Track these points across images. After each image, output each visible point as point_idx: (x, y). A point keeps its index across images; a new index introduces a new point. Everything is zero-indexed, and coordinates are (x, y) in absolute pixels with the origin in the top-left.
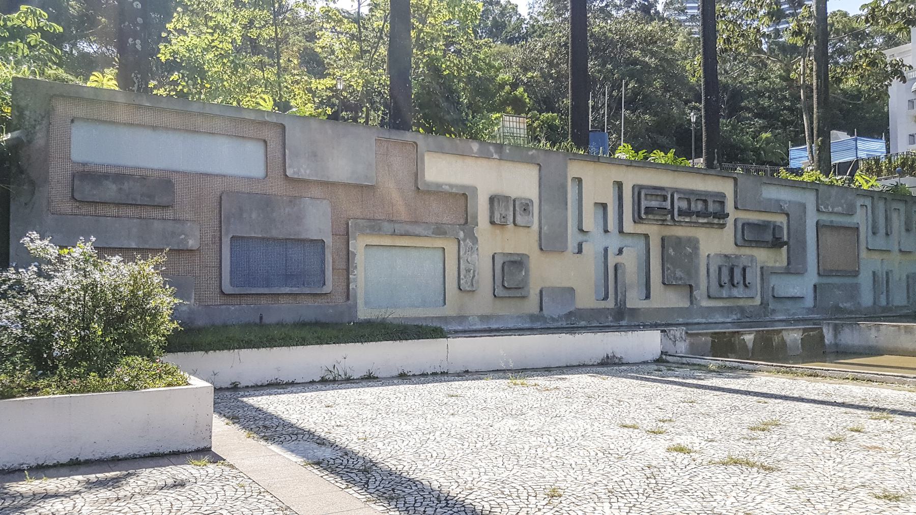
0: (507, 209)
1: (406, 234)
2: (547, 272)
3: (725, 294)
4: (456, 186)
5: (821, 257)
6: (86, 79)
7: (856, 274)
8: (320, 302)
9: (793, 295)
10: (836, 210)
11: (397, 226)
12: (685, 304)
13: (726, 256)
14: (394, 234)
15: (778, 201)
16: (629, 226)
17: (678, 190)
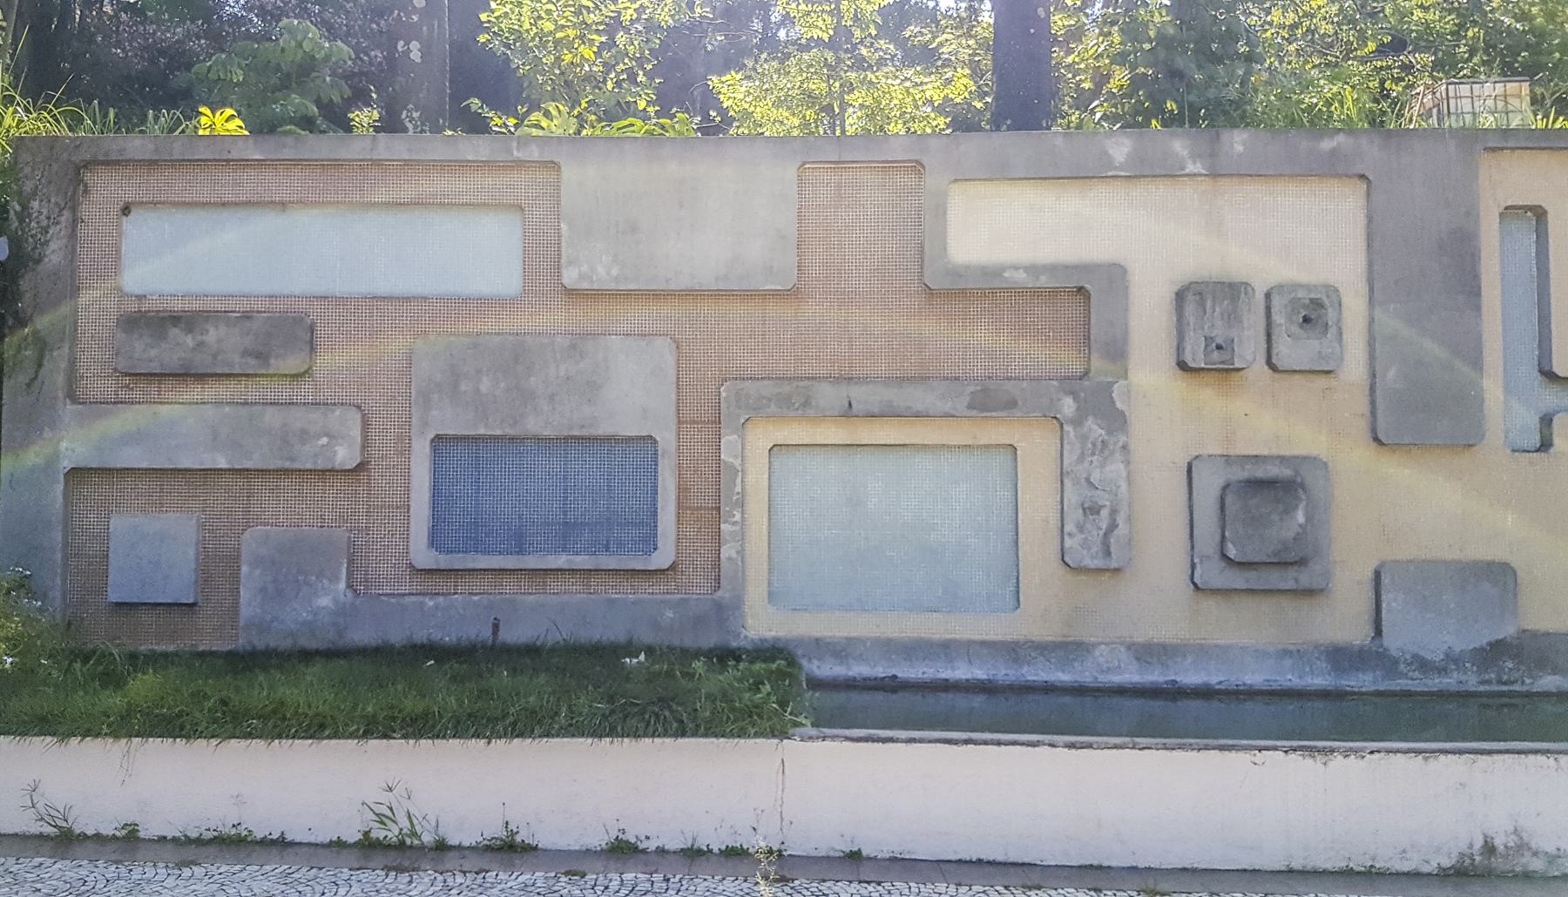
0: (1232, 318)
4: (1052, 269)
11: (858, 393)
14: (848, 413)
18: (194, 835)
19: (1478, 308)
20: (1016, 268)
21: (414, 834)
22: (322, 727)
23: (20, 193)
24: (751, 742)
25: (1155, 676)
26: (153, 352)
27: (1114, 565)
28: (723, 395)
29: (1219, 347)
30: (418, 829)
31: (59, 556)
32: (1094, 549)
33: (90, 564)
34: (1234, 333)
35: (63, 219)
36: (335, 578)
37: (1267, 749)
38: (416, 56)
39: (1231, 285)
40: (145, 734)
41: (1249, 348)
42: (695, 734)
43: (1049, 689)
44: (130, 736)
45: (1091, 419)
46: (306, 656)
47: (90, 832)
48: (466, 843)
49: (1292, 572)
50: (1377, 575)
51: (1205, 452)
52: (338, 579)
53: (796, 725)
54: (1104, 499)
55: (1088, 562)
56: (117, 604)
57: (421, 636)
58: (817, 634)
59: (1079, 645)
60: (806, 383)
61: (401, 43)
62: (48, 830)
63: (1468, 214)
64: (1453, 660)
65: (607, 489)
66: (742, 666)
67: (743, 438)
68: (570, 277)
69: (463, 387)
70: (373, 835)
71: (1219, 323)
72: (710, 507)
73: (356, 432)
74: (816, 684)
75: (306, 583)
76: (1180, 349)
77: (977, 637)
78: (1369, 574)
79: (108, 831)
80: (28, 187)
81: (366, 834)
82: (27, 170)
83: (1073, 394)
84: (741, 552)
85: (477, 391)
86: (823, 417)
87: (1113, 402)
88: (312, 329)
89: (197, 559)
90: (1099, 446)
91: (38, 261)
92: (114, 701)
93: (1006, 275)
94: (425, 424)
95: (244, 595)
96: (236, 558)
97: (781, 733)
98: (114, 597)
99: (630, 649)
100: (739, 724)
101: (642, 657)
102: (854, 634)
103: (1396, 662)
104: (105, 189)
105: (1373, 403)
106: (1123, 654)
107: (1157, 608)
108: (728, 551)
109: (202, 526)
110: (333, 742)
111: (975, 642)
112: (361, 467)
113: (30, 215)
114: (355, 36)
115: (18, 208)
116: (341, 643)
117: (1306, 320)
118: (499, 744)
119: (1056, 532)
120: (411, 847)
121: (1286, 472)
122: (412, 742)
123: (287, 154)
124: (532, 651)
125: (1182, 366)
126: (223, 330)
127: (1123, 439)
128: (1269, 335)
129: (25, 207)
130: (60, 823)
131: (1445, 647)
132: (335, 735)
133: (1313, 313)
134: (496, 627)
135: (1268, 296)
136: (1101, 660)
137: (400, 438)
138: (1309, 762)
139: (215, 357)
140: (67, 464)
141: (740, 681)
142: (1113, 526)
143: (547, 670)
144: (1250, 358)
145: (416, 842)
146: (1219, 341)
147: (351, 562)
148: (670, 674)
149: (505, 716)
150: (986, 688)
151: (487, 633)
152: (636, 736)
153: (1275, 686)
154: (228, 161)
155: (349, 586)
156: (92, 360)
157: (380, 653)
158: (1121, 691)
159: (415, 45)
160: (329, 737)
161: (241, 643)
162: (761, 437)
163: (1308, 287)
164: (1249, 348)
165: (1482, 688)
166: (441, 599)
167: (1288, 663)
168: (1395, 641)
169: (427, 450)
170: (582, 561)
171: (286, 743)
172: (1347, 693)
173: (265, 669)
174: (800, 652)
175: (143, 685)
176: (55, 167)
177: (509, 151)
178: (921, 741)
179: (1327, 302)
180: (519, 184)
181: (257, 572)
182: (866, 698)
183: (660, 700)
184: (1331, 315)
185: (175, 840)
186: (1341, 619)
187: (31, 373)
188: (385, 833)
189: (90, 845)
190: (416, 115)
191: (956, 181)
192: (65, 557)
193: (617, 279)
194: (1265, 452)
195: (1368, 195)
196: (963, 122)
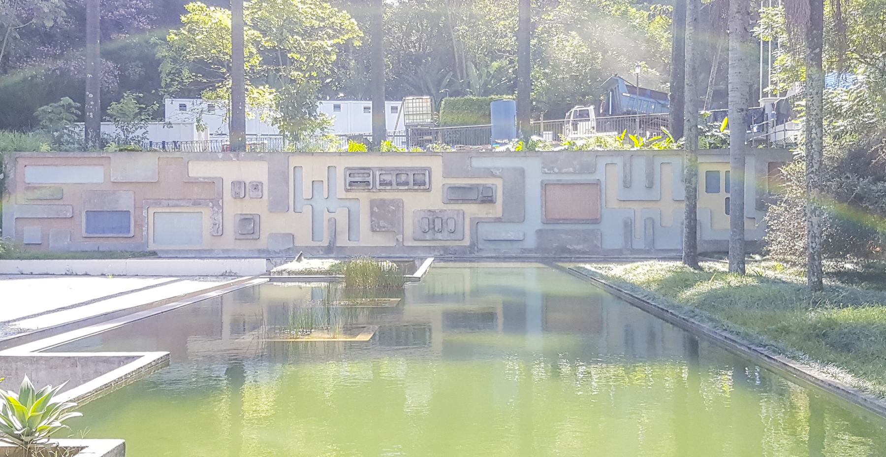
0: (240, 188)
1: (176, 206)
2: (273, 224)
3: (428, 237)
4: (208, 178)
5: (251, 255)
6: (690, 26)
7: (596, 221)
8: (128, 241)
9: (505, 238)
10: (564, 170)
11: (170, 202)
12: (393, 244)
13: (430, 211)
14: (168, 206)
15: (489, 169)
16: (341, 193)
17: (381, 169)
86: (163, 207)
104: (21, 162)
133: (257, 186)
170: (115, 235)
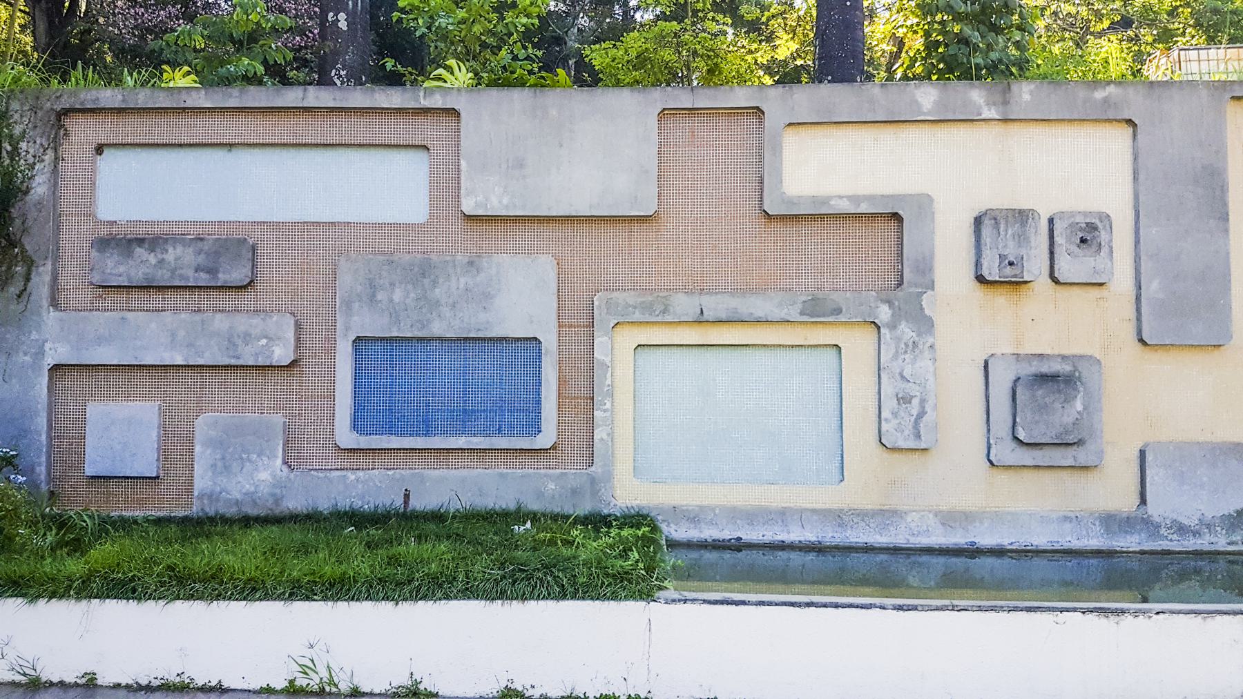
0: (1022, 239)
4: (870, 198)
14: (700, 321)
18: (144, 682)
19: (1226, 231)
20: (841, 197)
21: (331, 682)
22: (254, 589)
23: (11, 136)
24: (623, 603)
25: (958, 539)
26: (122, 269)
27: (923, 446)
28: (596, 303)
29: (1011, 264)
30: (336, 679)
31: (44, 437)
32: (907, 432)
33: (67, 440)
34: (1023, 252)
35: (46, 157)
36: (272, 456)
37: (1067, 610)
38: (343, 25)
39: (1020, 212)
40: (102, 595)
41: (1036, 267)
42: (574, 597)
43: (868, 549)
44: (90, 597)
45: (904, 324)
46: (247, 522)
47: (55, 680)
48: (377, 691)
49: (1070, 451)
50: (1142, 453)
51: (998, 351)
52: (276, 457)
53: (660, 588)
54: (914, 390)
55: (901, 444)
56: (92, 477)
57: (344, 504)
58: (674, 503)
59: (894, 513)
60: (665, 294)
61: (331, 14)
62: (18, 678)
63: (1217, 152)
64: (1208, 525)
65: (494, 384)
66: (614, 532)
67: (611, 338)
68: (468, 206)
69: (379, 297)
70: (298, 683)
71: (1011, 244)
72: (583, 399)
73: (290, 335)
74: (673, 545)
75: (249, 460)
76: (978, 265)
77: (809, 506)
78: (1137, 453)
79: (70, 679)
80: (17, 130)
81: (291, 682)
82: (17, 116)
83: (889, 302)
84: (611, 435)
85: (391, 301)
87: (922, 309)
88: (254, 248)
89: (159, 440)
90: (910, 344)
91: (26, 192)
92: (75, 566)
93: (832, 203)
94: (347, 329)
95: (198, 470)
96: (191, 441)
97: (647, 595)
98: (89, 471)
99: (519, 515)
100: (612, 588)
101: (528, 525)
102: (705, 503)
103: (1158, 526)
104: (82, 132)
105: (1138, 310)
106: (931, 520)
107: (962, 489)
108: (599, 434)
109: (162, 412)
110: (264, 603)
111: (806, 510)
112: (294, 363)
113: (19, 154)
114: (302, 17)
115: (9, 148)
116: (277, 512)
117: (1083, 241)
118: (405, 606)
119: (876, 419)
120: (330, 694)
121: (1067, 368)
122: (330, 603)
123: (233, 103)
124: (437, 517)
125: (980, 279)
126: (179, 250)
127: (931, 340)
128: (1052, 253)
129: (15, 148)
130: (28, 671)
131: (1198, 515)
132: (267, 597)
133: (1089, 235)
134: (407, 497)
135: (1051, 221)
136: (913, 525)
137: (328, 339)
138: (1103, 620)
139: (173, 271)
140: (50, 361)
141: (612, 547)
142: (922, 414)
143: (448, 538)
144: (1037, 273)
145: (334, 690)
146: (1012, 259)
147: (286, 442)
148: (552, 542)
149: (410, 582)
150: (817, 548)
151: (399, 502)
152: (524, 598)
153: (1057, 547)
154: (184, 109)
155: (285, 463)
156: (71, 273)
157: (311, 519)
158: (929, 551)
159: (342, 16)
160: (260, 599)
161: (195, 510)
162: (628, 338)
163: (1085, 214)
164: (1036, 267)
165: (1231, 548)
166: (360, 473)
167: (1068, 526)
168: (1155, 509)
169: (350, 349)
171: (223, 604)
172: (1116, 552)
173: (208, 536)
174: (660, 518)
175: (102, 553)
176: (40, 114)
177: (418, 100)
178: (770, 604)
179: (1100, 225)
180: (427, 130)
181: (209, 451)
182: (710, 556)
183: (545, 566)
184: (1103, 236)
185: (128, 687)
186: (1112, 490)
187: (21, 286)
188: (307, 681)
189: (55, 690)
190: (342, 73)
191: (790, 124)
192: (50, 438)
193: (507, 207)
194: (1049, 352)
195: (1135, 136)
196: (787, 76)
